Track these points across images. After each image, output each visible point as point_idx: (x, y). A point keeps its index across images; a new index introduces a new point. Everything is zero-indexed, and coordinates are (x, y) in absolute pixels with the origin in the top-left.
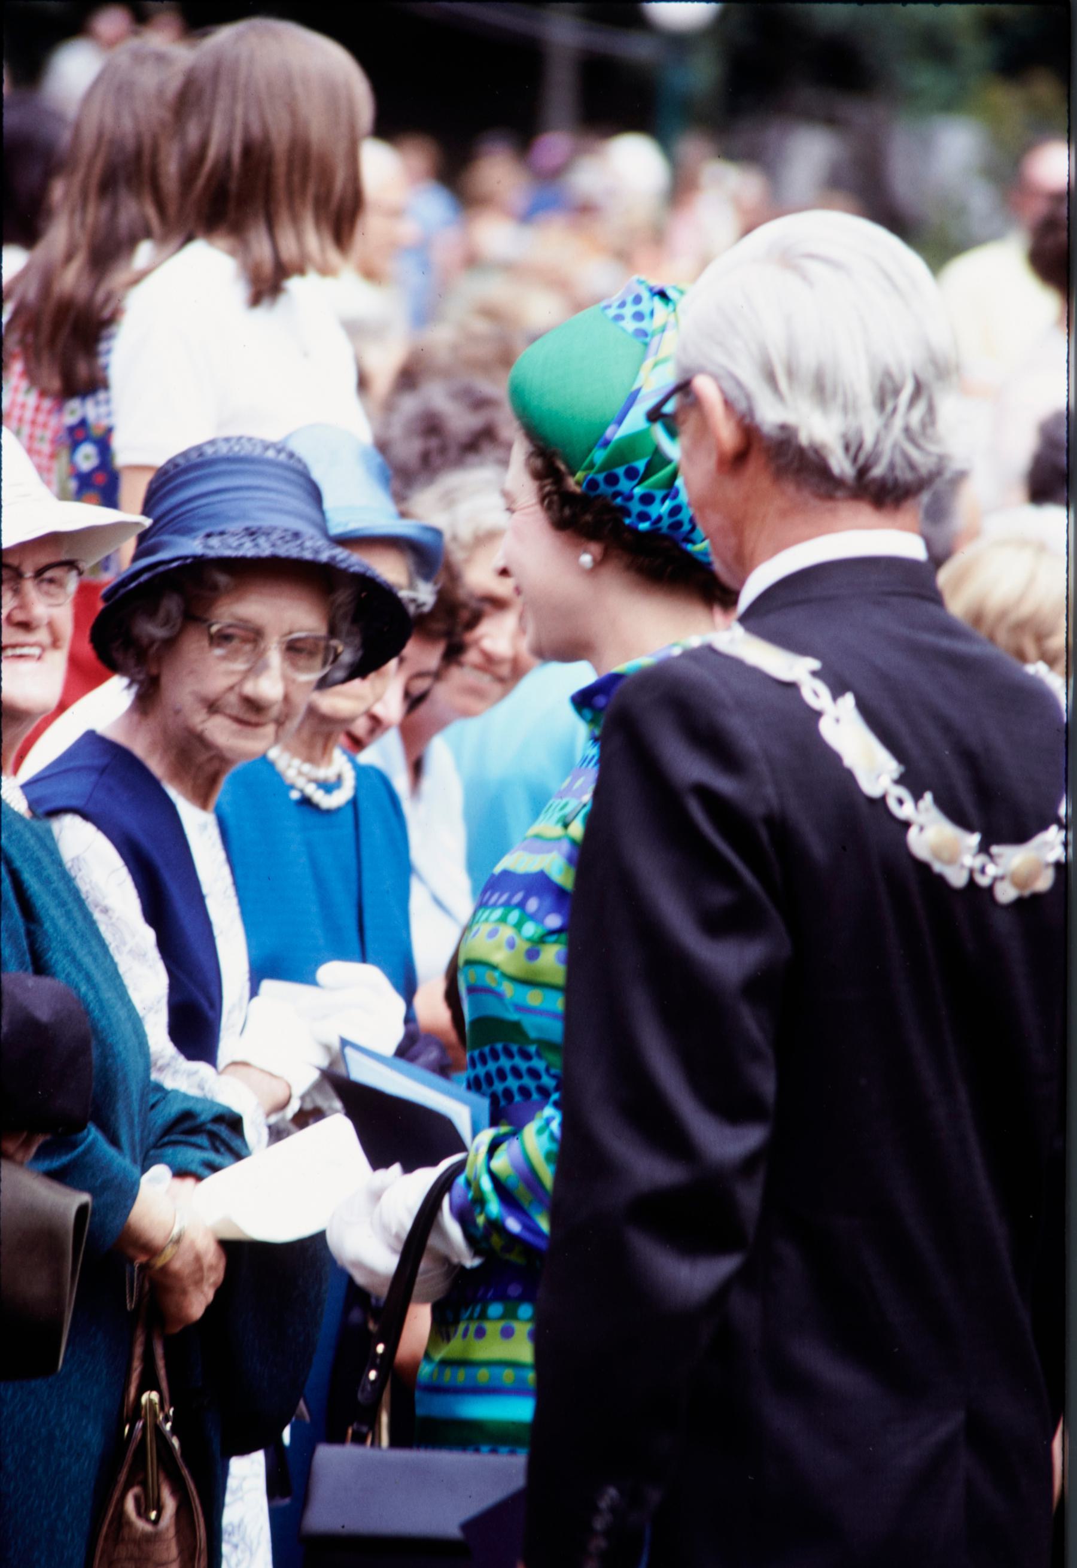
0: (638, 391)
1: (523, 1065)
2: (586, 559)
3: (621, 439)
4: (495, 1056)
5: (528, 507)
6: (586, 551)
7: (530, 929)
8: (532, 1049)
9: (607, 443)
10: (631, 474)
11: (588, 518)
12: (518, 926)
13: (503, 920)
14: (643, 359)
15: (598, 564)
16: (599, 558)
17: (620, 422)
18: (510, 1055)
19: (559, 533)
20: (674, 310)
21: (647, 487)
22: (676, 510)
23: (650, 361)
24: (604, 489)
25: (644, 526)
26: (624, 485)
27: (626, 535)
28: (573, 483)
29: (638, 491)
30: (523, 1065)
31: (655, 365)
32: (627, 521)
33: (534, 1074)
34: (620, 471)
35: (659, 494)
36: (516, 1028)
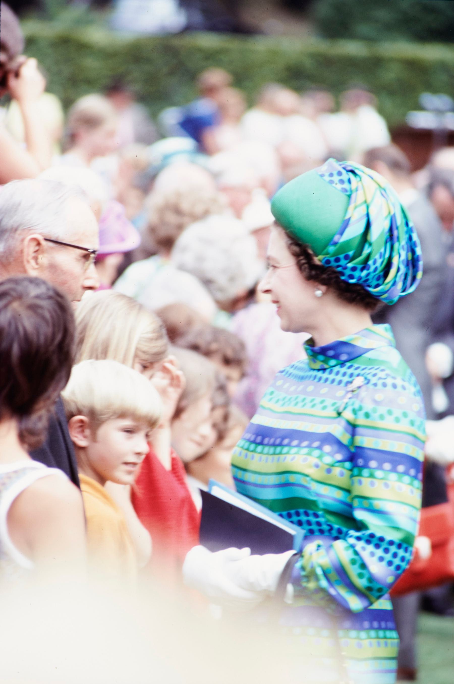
0: (349, 219)
1: (313, 519)
2: (319, 293)
4: (298, 514)
5: (287, 267)
6: (319, 289)
7: (328, 460)
8: (320, 513)
9: (335, 244)
10: (347, 257)
11: (325, 276)
12: (320, 457)
13: (309, 454)
14: (349, 203)
15: (324, 294)
16: (324, 291)
17: (342, 233)
18: (307, 514)
19: (309, 282)
20: (361, 180)
21: (355, 264)
22: (368, 275)
23: (352, 206)
24: (333, 264)
25: (352, 281)
26: (343, 262)
27: (342, 284)
28: (318, 260)
29: (350, 265)
30: (313, 519)
31: (356, 207)
32: (343, 278)
33: (319, 524)
34: (342, 256)
35: (360, 267)
36: (313, 503)
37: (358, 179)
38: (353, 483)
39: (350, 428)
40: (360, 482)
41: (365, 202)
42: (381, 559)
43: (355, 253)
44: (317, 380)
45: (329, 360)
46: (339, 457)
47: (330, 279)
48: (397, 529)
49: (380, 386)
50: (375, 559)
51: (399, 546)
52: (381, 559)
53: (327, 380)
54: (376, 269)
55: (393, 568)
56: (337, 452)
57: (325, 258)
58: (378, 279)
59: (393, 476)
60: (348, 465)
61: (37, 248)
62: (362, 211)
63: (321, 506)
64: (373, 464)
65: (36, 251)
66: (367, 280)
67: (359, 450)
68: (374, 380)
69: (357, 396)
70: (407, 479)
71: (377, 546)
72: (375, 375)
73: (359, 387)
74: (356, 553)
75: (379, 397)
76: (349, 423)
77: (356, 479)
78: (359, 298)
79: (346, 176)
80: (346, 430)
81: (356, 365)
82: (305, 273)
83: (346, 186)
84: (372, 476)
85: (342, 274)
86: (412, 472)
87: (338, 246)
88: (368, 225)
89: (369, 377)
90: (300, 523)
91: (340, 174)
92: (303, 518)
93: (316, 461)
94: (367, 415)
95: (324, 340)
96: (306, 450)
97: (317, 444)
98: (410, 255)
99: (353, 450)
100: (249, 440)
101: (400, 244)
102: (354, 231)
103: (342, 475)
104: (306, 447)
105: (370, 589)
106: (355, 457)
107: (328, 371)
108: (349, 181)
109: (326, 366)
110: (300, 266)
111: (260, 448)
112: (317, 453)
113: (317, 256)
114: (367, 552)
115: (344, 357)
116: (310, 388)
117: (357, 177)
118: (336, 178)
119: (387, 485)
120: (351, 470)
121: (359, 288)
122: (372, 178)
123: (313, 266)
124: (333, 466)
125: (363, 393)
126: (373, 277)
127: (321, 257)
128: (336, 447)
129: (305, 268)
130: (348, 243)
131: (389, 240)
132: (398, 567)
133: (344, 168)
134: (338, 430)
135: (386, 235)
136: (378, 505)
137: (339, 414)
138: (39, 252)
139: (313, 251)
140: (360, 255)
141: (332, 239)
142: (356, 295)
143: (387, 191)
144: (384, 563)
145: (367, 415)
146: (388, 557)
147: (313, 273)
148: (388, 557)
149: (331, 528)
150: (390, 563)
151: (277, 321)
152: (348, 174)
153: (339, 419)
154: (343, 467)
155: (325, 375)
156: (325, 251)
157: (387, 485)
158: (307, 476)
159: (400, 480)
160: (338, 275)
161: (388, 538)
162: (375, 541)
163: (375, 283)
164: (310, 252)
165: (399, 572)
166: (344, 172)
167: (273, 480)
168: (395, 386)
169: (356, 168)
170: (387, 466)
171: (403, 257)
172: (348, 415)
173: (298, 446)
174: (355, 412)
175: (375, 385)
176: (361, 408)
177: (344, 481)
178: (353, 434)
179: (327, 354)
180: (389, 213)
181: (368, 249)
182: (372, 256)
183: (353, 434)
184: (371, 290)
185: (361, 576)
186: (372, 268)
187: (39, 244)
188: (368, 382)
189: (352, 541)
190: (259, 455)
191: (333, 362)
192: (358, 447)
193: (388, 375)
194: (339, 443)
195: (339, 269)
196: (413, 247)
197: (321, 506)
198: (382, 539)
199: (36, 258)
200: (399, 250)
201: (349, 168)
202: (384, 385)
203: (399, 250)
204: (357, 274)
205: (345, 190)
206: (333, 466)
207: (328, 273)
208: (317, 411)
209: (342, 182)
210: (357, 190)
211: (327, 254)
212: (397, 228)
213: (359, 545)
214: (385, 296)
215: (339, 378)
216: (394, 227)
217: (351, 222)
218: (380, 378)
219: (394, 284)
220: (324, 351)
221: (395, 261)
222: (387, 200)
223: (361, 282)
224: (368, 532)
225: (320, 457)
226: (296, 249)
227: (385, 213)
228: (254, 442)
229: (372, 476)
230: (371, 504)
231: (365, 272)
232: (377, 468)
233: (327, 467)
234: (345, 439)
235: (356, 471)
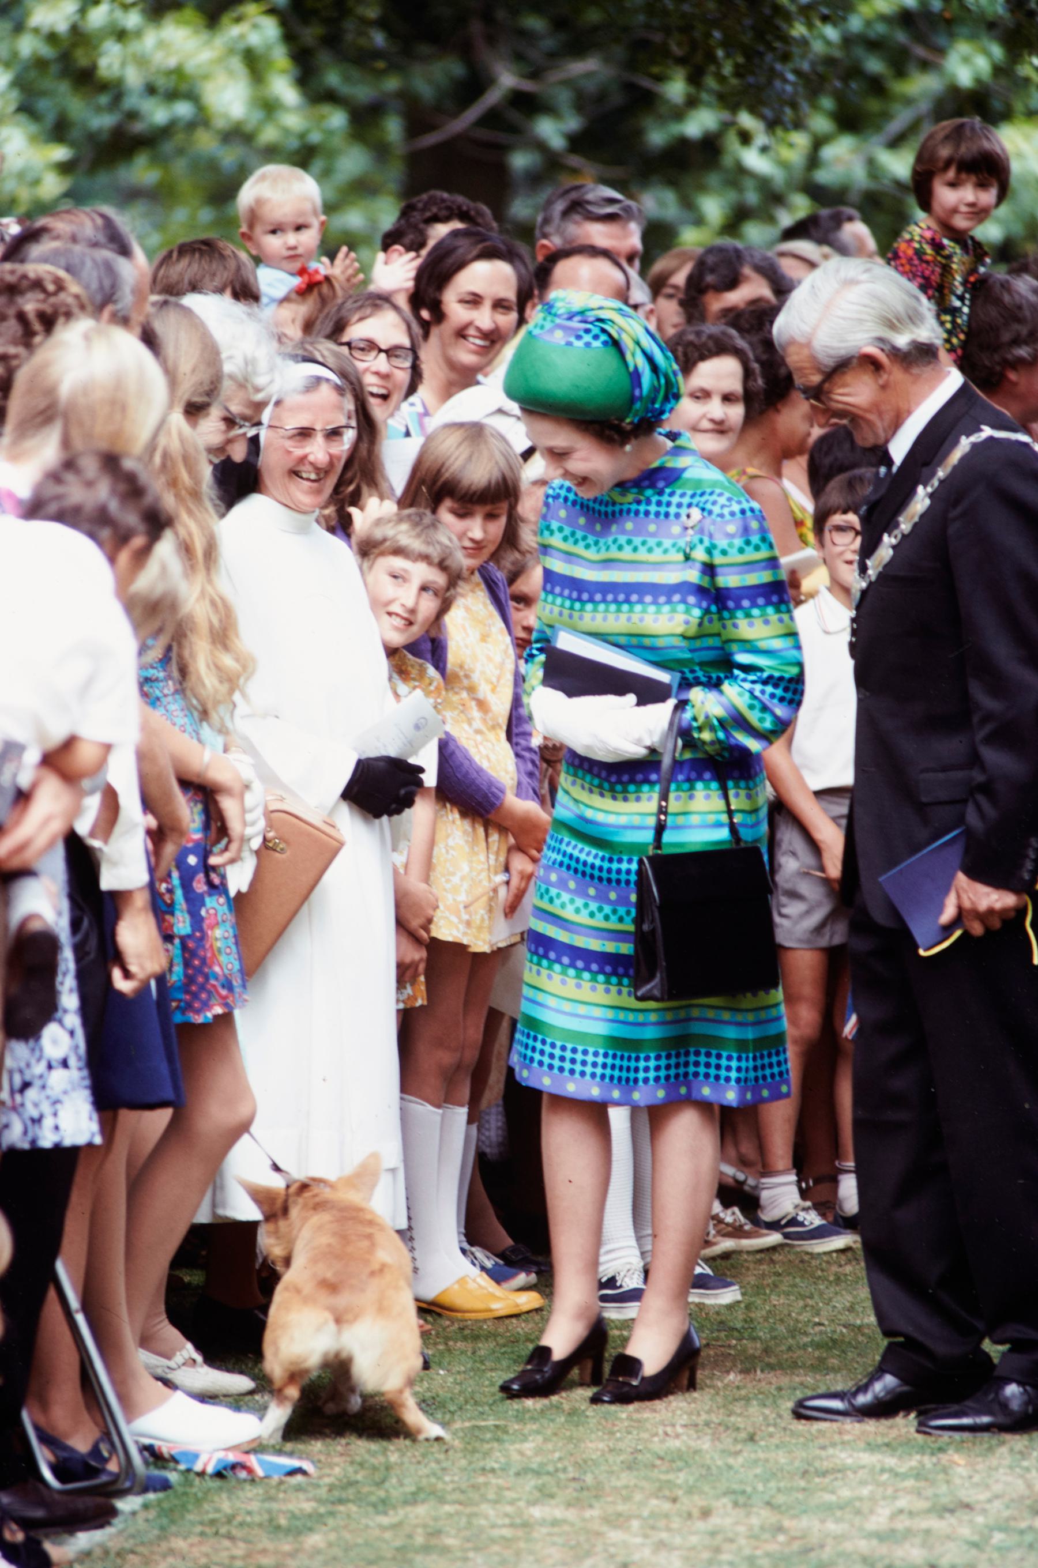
13: (674, 611)
40: (735, 626)
50: (776, 701)
72: (714, 503)
89: (708, 506)
94: (724, 553)
134: (693, 575)
137: (687, 558)
145: (724, 553)
153: (690, 563)
176: (714, 546)
188: (710, 512)
218: (723, 507)
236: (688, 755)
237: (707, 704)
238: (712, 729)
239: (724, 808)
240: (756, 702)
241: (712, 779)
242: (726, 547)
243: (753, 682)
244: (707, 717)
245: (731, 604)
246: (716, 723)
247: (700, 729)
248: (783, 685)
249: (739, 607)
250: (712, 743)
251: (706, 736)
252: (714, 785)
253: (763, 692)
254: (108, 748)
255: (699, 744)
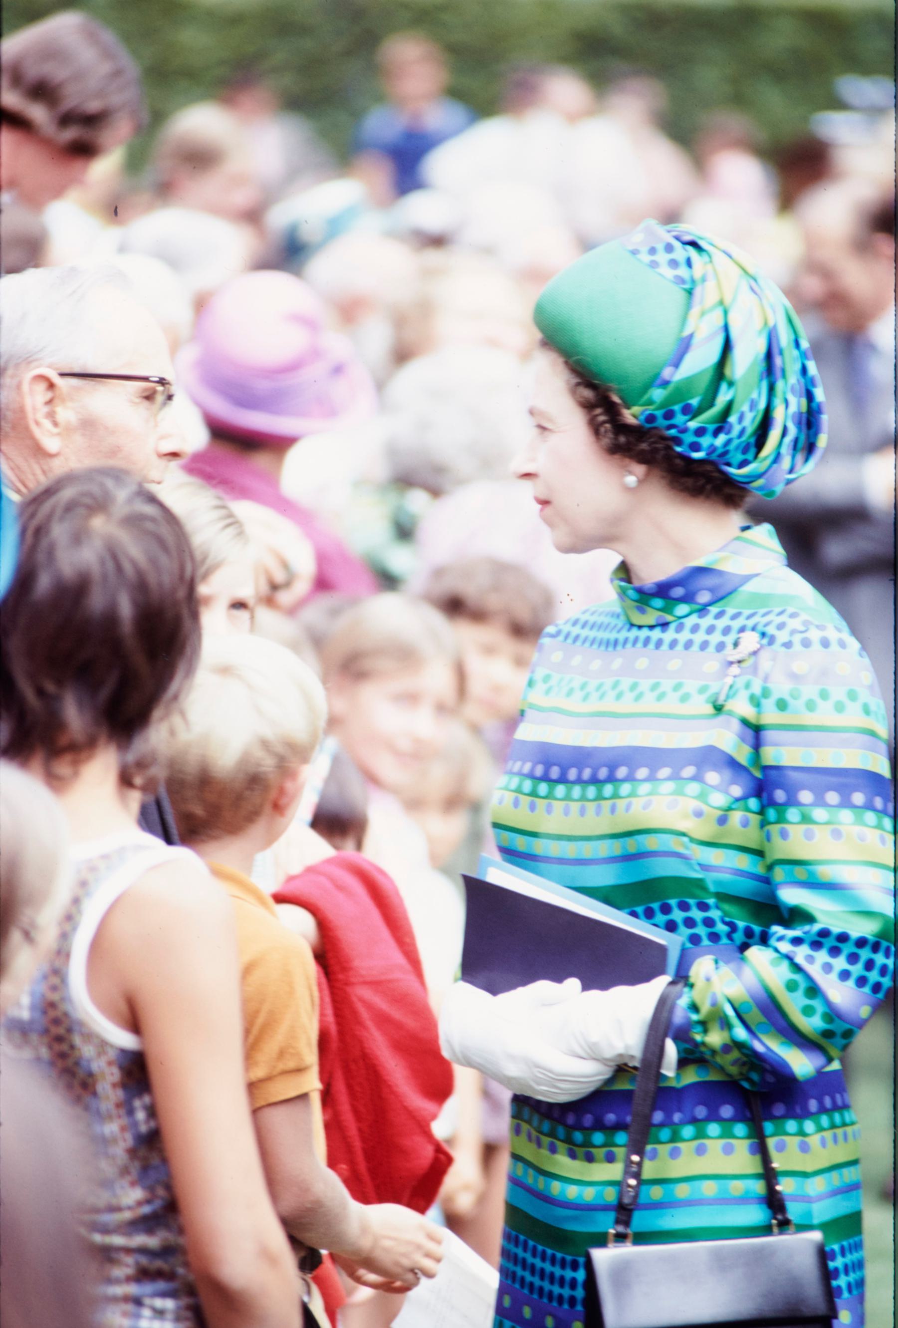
0: (691, 336)
1: (697, 914)
2: (631, 480)
3: (679, 382)
7: (719, 799)
8: (711, 901)
9: (665, 383)
10: (687, 410)
11: (644, 446)
12: (702, 797)
13: (679, 792)
14: (689, 306)
15: (640, 482)
17: (676, 364)
20: (711, 262)
22: (728, 442)
23: (695, 311)
24: (661, 422)
25: (696, 455)
26: (679, 419)
27: (678, 461)
28: (631, 416)
29: (693, 425)
30: (697, 914)
31: (703, 314)
32: (678, 449)
33: (709, 923)
34: (677, 408)
35: (711, 427)
36: (700, 884)
37: (705, 257)
38: (769, 838)
39: (750, 734)
40: (784, 835)
41: (721, 302)
42: (845, 975)
43: (701, 402)
44: (640, 644)
45: (675, 605)
46: (737, 791)
47: (655, 451)
48: (868, 914)
49: (797, 647)
50: (834, 976)
51: (876, 948)
52: (845, 975)
53: (673, 644)
54: (742, 432)
55: (867, 990)
56: (733, 782)
57: (646, 410)
58: (745, 451)
59: (846, 815)
60: (753, 803)
61: (49, 395)
62: (715, 320)
63: (712, 888)
64: (806, 796)
65: (49, 402)
66: (725, 453)
67: (773, 773)
68: (782, 637)
69: (755, 670)
70: (870, 817)
71: (835, 952)
72: (781, 626)
73: (755, 653)
74: (798, 968)
75: (800, 666)
76: (745, 722)
77: (775, 829)
78: (709, 487)
79: (681, 253)
80: (743, 739)
81: (731, 611)
82: (606, 441)
83: (683, 271)
84: (806, 819)
85: (678, 441)
86: (878, 802)
87: (670, 388)
88: (727, 347)
89: (771, 630)
90: (671, 927)
91: (669, 248)
92: (678, 915)
93: (695, 804)
94: (782, 705)
95: (655, 569)
96: (670, 786)
97: (689, 771)
98: (804, 401)
99: (758, 774)
100: (531, 776)
101: (786, 383)
102: (700, 360)
103: (745, 824)
104: (669, 779)
105: (828, 1034)
106: (766, 788)
107: (673, 626)
108: (689, 263)
109: (669, 618)
110: (595, 428)
111: (560, 790)
112: (694, 788)
113: (628, 407)
114: (817, 963)
115: (704, 597)
116: (642, 663)
117: (704, 253)
118: (662, 257)
119: (837, 834)
120: (761, 812)
121: (709, 468)
122: (730, 257)
123: (620, 427)
124: (729, 809)
125: (765, 661)
126: (737, 448)
127: (636, 409)
128: (728, 774)
129: (606, 432)
130: (689, 381)
131: (765, 375)
132: (877, 987)
133: (677, 238)
134: (728, 739)
135: (761, 367)
136: (827, 873)
137: (719, 709)
138: (56, 401)
139: (621, 398)
140: (711, 404)
141: (657, 375)
142: (706, 482)
143: (759, 281)
144: (851, 983)
145: (782, 705)
146: (857, 970)
147: (622, 439)
148: (857, 970)
149: (733, 927)
150: (861, 981)
151: (547, 537)
152: (686, 250)
153: (721, 718)
154: (748, 810)
155: (669, 635)
156: (646, 397)
157: (837, 834)
158: (684, 834)
159: (860, 821)
160: (670, 443)
161: (855, 934)
162: (829, 942)
163: (739, 457)
164: (616, 399)
165: (880, 996)
166: (677, 244)
167: (605, 849)
168: (825, 643)
169: (701, 239)
170: (832, 797)
171: (793, 408)
172: (742, 708)
173: (651, 778)
174: (755, 702)
175: (788, 645)
176: (766, 693)
177: (752, 837)
178: (757, 745)
179: (662, 598)
180: (766, 323)
181: (726, 393)
182: (735, 407)
183: (757, 745)
184: (732, 470)
185: (808, 1011)
186: (736, 429)
187: (51, 386)
188: (772, 640)
189: (785, 947)
190: (563, 803)
191: (682, 609)
192: (766, 769)
193: (806, 623)
194: (733, 763)
195: (673, 432)
196: (810, 388)
197: (712, 888)
198: (843, 938)
199: (51, 415)
200: (784, 393)
201: (688, 238)
202: (806, 643)
203: (784, 393)
204: (706, 441)
205: (680, 280)
206: (729, 809)
207: (652, 440)
208: (671, 705)
209: (674, 263)
210: (704, 279)
211: (650, 402)
212: (781, 353)
213: (801, 953)
214: (760, 482)
215: (715, 638)
216: (775, 351)
217: (695, 341)
218: (793, 632)
219: (777, 458)
220: (663, 590)
221: (779, 414)
222: (760, 299)
223: (714, 457)
224: (816, 927)
225: (702, 797)
226: (588, 394)
227: (758, 324)
228: (545, 778)
229: (806, 819)
230: (811, 874)
231: (722, 438)
232: (815, 804)
233: (721, 813)
234: (743, 755)
235: (771, 813)
236: (691, 1077)
237: (721, 981)
238: (725, 1024)
239: (759, 1170)
240: (798, 977)
241: (737, 1118)
242: (787, 698)
243: (797, 941)
244: (714, 1004)
245: (780, 795)
246: (730, 1012)
247: (704, 1025)
248: (848, 948)
249: (792, 801)
250: (726, 1049)
251: (715, 1038)
252: (740, 1129)
253: (810, 959)
254: (717, 968)
255: (708, 1056)
